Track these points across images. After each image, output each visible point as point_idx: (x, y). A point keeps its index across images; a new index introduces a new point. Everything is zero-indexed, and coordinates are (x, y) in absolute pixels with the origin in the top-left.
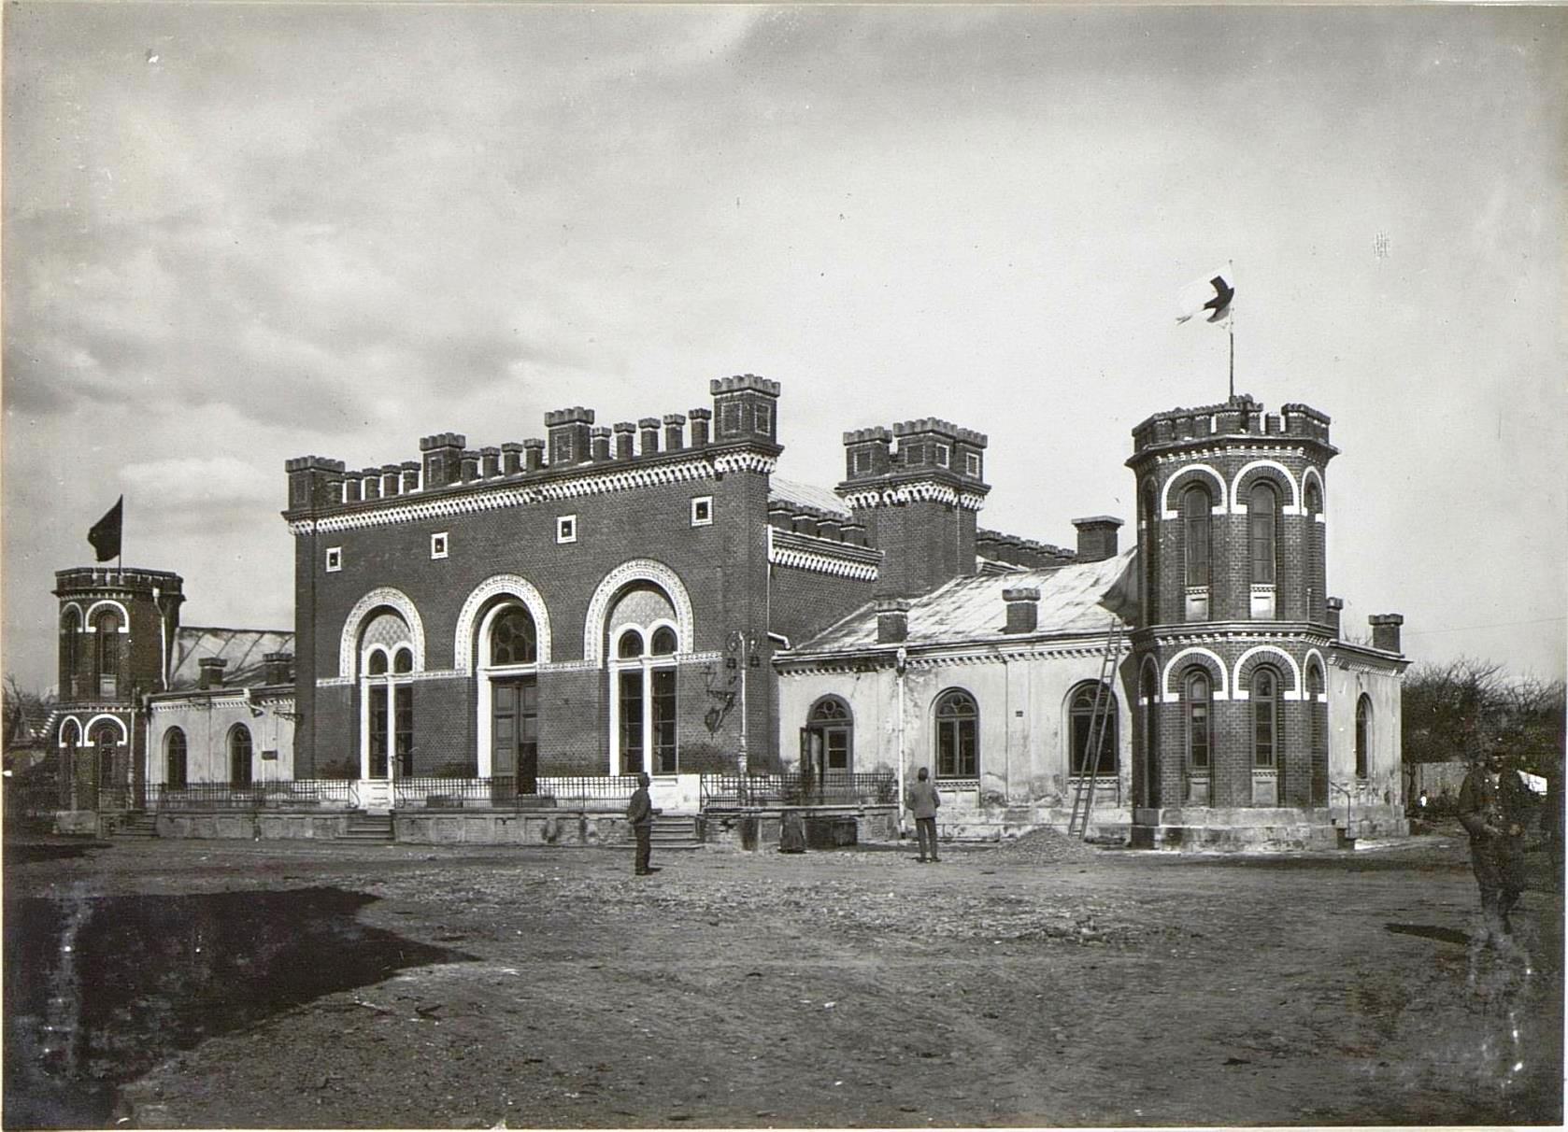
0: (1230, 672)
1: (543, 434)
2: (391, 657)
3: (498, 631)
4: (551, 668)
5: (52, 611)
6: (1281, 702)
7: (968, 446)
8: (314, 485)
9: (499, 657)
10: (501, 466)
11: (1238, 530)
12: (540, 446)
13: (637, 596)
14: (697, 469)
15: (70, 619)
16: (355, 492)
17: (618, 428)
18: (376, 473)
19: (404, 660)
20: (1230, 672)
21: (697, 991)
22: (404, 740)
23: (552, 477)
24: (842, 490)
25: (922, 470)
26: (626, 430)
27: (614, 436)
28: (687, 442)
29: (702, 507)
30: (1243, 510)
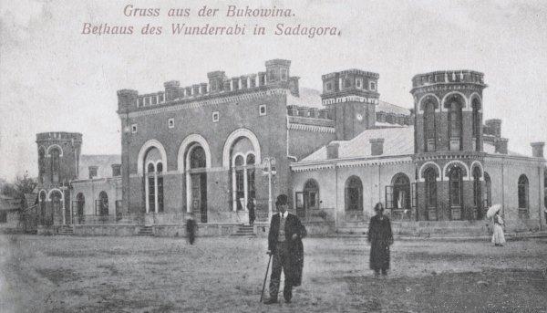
0: (442, 170)
1: (206, 81)
2: (245, 157)
3: (193, 158)
4: (167, 173)
5: (35, 147)
6: (462, 181)
7: (370, 78)
8: (127, 100)
9: (193, 166)
10: (200, 91)
11: (444, 118)
12: (206, 85)
13: (238, 146)
14: (260, 94)
15: (41, 153)
16: (141, 104)
17: (234, 79)
18: (148, 95)
19: (160, 166)
20: (442, 170)
21: (92, 255)
22: (161, 199)
23: (210, 97)
24: (324, 97)
25: (351, 88)
26: (236, 80)
27: (240, 81)
28: (257, 84)
29: (263, 109)
30: (446, 110)
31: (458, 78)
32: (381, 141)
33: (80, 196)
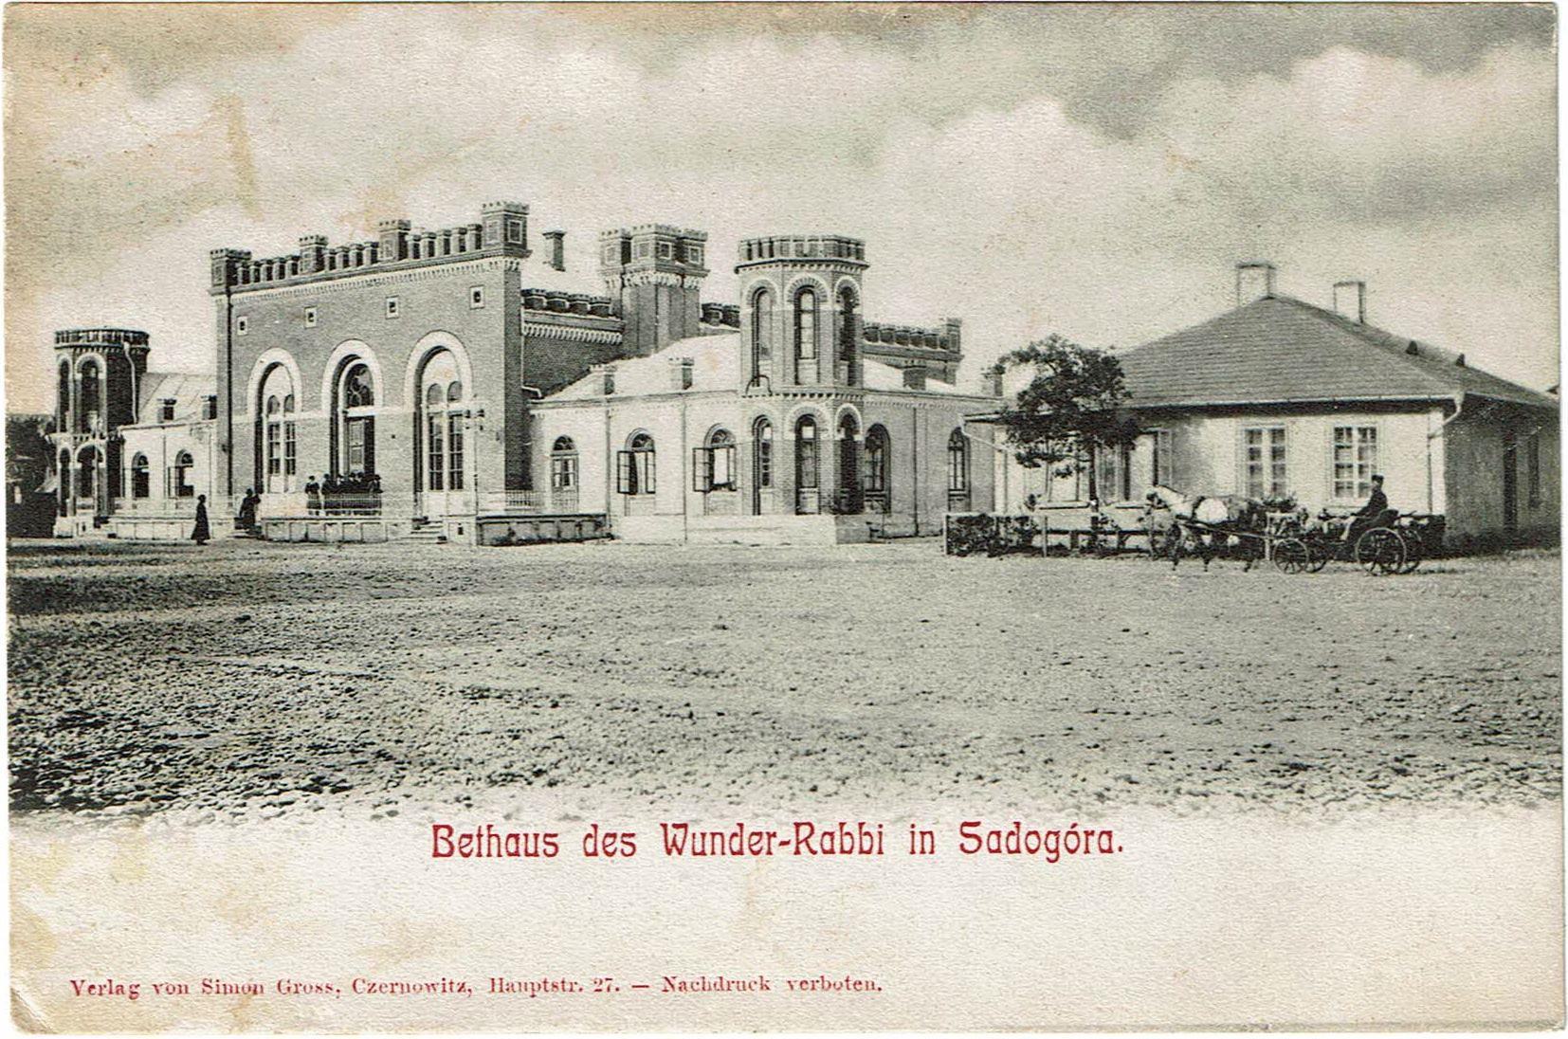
31: (813, 249)
32: (687, 363)
33: (141, 460)
